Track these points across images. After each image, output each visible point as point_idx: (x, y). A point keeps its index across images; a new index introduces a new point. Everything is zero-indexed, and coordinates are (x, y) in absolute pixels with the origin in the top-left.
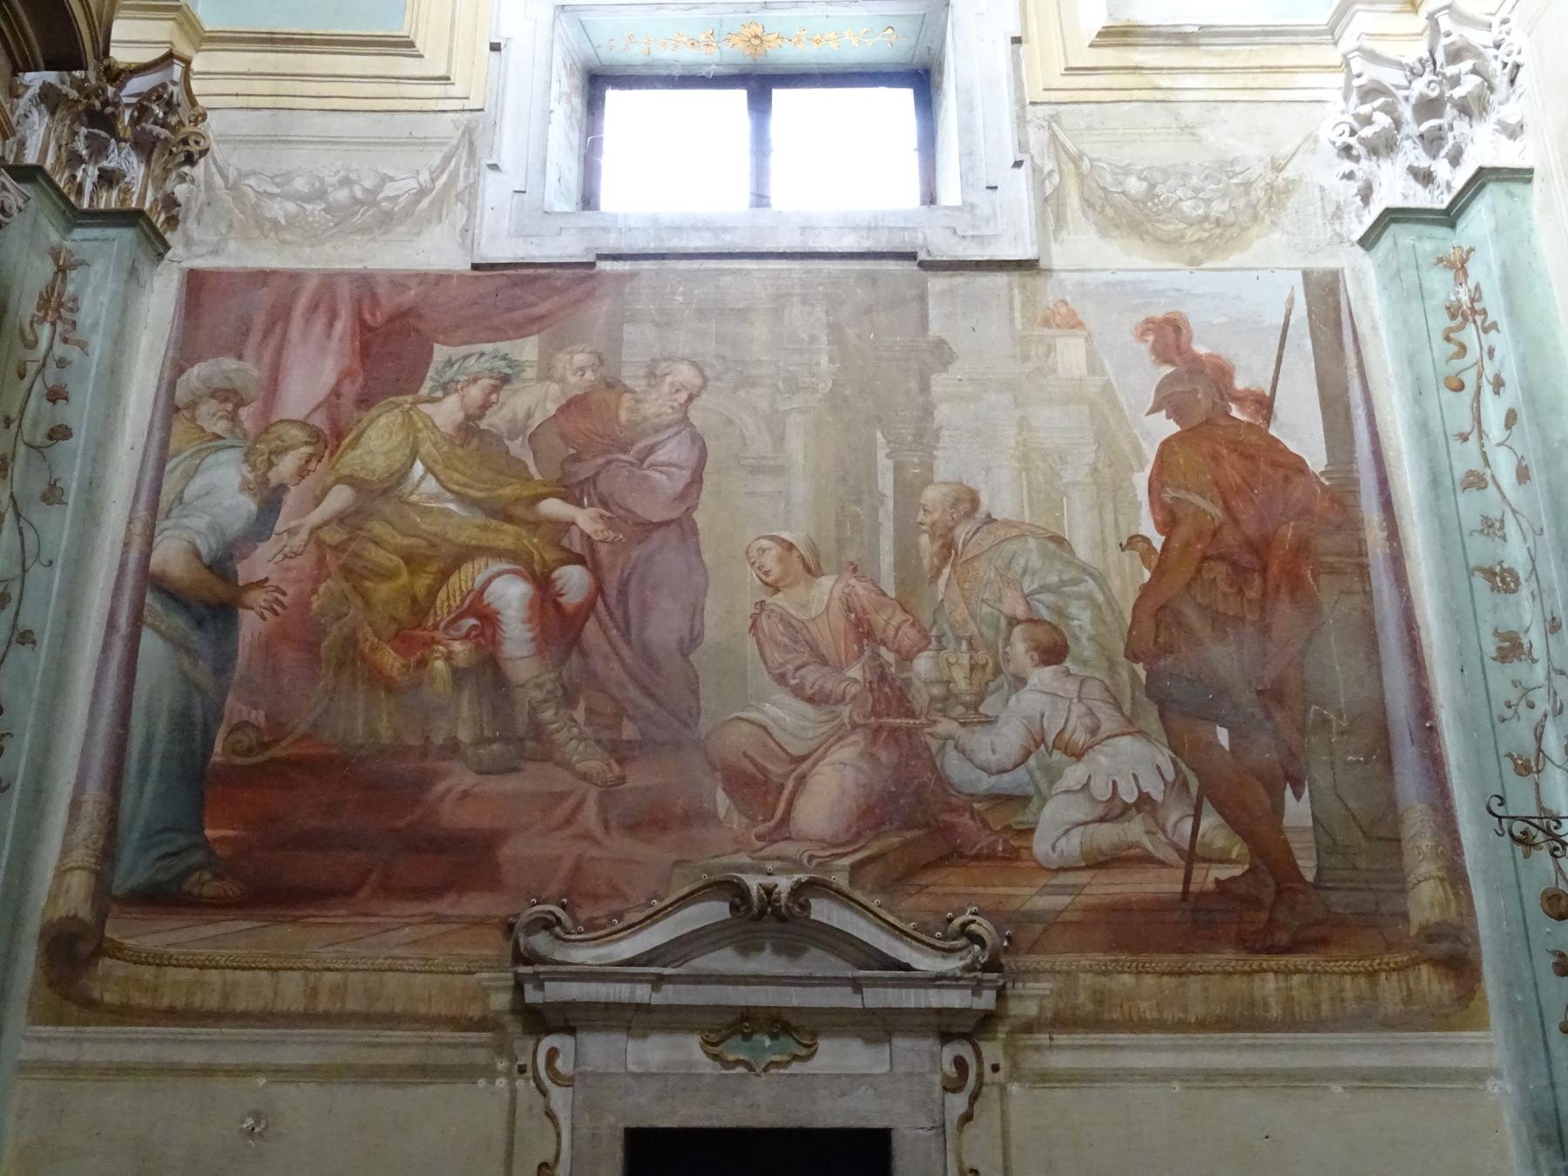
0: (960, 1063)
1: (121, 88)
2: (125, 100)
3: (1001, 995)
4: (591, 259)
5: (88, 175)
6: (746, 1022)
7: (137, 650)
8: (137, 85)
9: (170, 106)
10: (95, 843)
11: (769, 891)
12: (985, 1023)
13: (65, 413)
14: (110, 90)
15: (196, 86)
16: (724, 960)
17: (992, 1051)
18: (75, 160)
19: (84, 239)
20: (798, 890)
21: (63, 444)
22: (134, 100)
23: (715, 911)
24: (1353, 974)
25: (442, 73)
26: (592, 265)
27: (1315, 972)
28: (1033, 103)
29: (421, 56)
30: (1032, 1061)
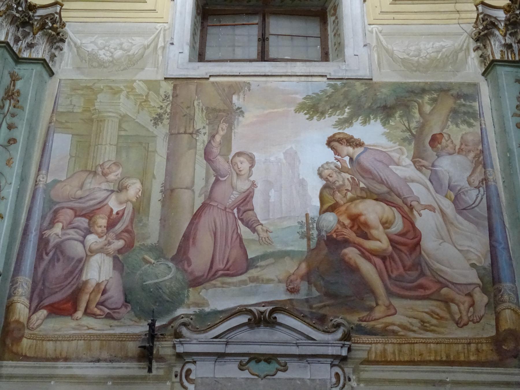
0: (337, 374)
1: (34, 13)
2: (36, 18)
3: (349, 350)
4: (208, 77)
5: (23, 44)
6: (256, 358)
7: (6, 258)
8: (41, 12)
9: (54, 21)
10: (475, 35)
11: (262, 313)
12: (344, 359)
13: (15, 134)
14: (31, 13)
15: (63, 14)
16: (246, 335)
17: (348, 370)
18: (17, 40)
19: (22, 70)
20: (272, 312)
21: (13, 146)
22: (39, 18)
23: (243, 319)
24: (106, 341)
25: (153, 8)
26: (208, 79)
27: (90, 340)
28: (370, 25)
29: (146, 2)
30: (364, 375)
